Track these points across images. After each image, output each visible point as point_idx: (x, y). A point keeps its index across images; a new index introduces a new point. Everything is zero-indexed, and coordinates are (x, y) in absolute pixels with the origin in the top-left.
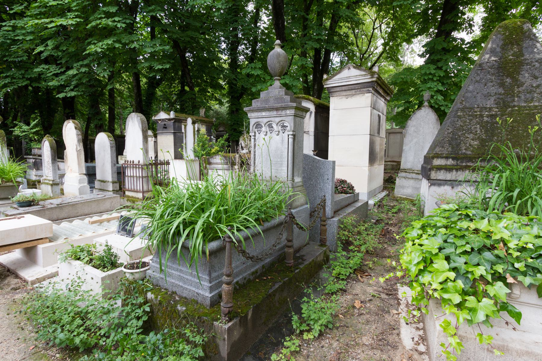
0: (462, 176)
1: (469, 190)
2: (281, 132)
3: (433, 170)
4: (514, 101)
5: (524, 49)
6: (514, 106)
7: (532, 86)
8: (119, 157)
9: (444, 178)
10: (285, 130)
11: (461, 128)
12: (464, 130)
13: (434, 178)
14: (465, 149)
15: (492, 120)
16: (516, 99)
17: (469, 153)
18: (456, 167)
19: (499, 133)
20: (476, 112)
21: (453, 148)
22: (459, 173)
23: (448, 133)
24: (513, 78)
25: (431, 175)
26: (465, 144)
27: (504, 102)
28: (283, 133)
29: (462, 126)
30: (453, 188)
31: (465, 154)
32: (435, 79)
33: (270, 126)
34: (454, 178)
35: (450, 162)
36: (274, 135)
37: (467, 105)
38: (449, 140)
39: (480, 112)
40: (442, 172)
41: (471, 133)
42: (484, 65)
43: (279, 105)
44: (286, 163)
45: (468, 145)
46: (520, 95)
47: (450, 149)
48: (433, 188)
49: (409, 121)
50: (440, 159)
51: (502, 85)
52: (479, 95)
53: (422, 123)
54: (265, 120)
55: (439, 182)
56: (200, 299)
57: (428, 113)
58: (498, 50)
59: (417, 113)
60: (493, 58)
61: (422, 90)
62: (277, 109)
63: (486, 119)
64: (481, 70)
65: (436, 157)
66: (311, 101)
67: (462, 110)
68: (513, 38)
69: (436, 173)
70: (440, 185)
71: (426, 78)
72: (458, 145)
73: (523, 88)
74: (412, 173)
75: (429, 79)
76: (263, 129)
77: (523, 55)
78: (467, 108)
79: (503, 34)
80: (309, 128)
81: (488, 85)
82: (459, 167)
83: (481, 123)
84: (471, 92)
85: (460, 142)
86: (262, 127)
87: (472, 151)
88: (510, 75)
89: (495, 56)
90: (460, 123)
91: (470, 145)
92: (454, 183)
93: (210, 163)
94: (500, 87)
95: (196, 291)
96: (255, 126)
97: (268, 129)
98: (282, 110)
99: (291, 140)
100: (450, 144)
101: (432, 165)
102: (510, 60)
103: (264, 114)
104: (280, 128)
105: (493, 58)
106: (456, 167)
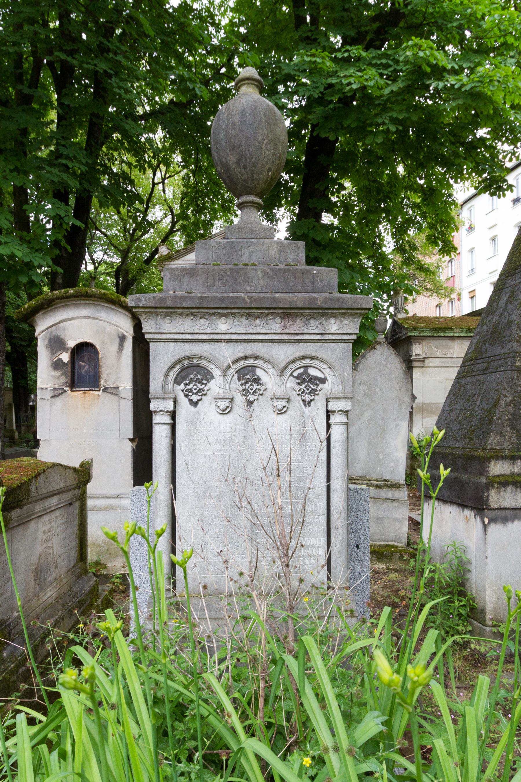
2: (297, 401)
3: (493, 487)
10: (313, 392)
13: (497, 506)
38: (509, 419)
40: (509, 489)
44: (323, 519)
47: (514, 439)
48: (495, 529)
50: (501, 462)
53: (379, 378)
55: (503, 513)
57: (387, 358)
69: (498, 493)
70: (505, 520)
80: (118, 378)
86: (208, 376)
96: (173, 374)
97: (236, 385)
100: (513, 428)
101: (488, 477)
104: (292, 383)
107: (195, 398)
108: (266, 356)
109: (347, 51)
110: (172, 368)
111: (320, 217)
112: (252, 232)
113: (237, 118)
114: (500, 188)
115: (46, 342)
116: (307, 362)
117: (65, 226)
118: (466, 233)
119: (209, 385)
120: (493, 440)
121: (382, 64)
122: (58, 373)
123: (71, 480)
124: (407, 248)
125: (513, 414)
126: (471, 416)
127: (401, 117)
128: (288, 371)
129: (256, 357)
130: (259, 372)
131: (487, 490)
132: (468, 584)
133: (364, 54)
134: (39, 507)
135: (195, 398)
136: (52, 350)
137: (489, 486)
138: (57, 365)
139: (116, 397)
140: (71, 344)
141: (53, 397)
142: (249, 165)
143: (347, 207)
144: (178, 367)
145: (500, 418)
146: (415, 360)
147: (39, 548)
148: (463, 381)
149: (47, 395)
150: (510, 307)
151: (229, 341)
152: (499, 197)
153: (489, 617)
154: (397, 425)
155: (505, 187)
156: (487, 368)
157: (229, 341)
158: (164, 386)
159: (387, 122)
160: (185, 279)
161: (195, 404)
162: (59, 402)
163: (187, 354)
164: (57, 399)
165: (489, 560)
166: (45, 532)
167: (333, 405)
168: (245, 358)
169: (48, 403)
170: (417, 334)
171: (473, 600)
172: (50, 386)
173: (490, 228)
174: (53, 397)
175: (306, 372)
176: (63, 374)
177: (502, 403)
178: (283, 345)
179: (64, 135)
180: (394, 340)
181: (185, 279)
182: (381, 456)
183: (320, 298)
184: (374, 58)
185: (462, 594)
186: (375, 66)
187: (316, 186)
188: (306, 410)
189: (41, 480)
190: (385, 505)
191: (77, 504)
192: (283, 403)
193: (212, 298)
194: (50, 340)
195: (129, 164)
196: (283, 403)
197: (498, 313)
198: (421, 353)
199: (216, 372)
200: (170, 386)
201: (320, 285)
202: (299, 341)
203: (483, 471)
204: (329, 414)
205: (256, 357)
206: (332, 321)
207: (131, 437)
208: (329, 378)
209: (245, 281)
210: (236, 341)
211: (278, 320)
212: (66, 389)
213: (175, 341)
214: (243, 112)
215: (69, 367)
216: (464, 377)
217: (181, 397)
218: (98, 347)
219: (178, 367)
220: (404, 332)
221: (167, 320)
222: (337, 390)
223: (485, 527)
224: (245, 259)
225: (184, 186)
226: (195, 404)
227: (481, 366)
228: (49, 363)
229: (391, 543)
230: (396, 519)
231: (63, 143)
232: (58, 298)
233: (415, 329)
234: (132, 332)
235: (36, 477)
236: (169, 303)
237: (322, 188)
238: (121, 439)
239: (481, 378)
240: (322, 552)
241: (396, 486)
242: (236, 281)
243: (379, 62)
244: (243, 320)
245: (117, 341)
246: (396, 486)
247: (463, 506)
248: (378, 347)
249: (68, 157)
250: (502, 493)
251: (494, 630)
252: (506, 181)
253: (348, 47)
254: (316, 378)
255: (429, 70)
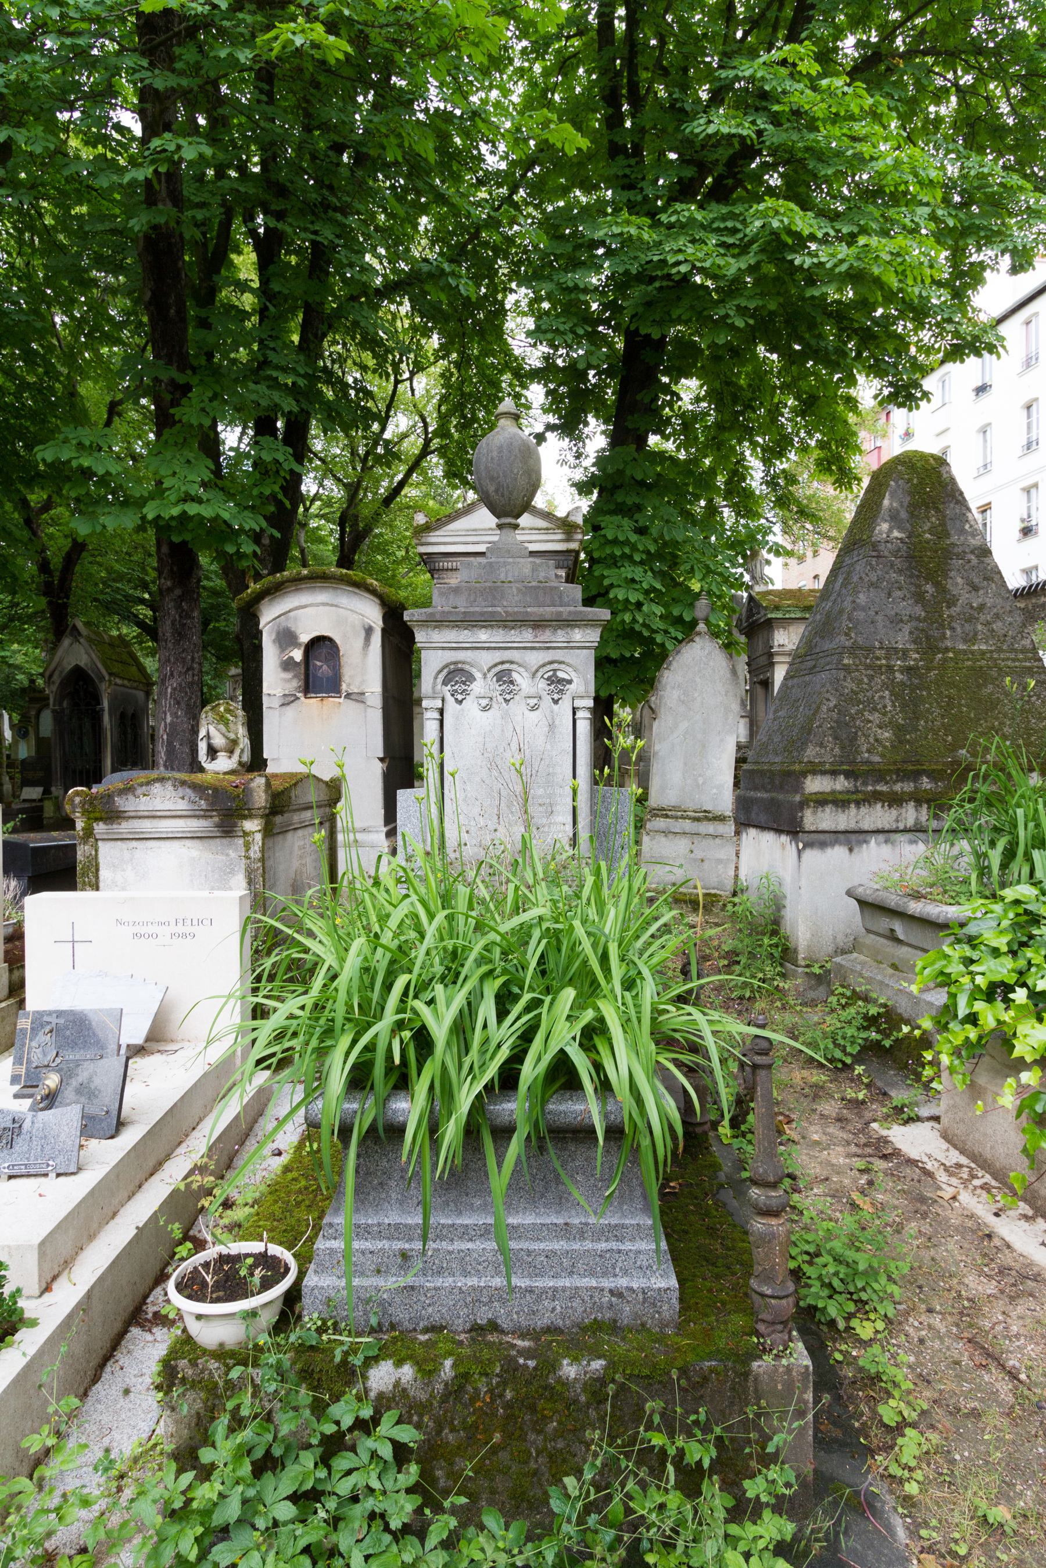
0: (878, 816)
1: (913, 851)
2: (547, 700)
4: (943, 637)
5: (949, 522)
6: (947, 650)
7: (972, 607)
8: (403, 796)
9: (833, 828)
10: (561, 691)
11: (852, 699)
12: (859, 702)
13: (813, 828)
14: (868, 751)
15: (910, 679)
16: (948, 632)
17: (877, 759)
18: (854, 797)
19: (928, 711)
20: (878, 659)
21: (842, 748)
22: (864, 810)
23: (829, 710)
24: (937, 584)
25: (805, 820)
26: (867, 736)
27: (928, 638)
28: (556, 702)
29: (856, 694)
30: (851, 850)
31: (868, 762)
32: (637, 558)
33: (504, 677)
34: (852, 826)
35: (841, 784)
36: (518, 707)
37: (860, 641)
38: (832, 728)
39: (887, 658)
40: (828, 809)
41: (875, 709)
42: (882, 547)
43: (548, 611)
45: (872, 740)
46: (954, 624)
47: (837, 751)
48: (810, 855)
49: (666, 673)
51: (919, 597)
52: (879, 618)
53: (698, 680)
54: (487, 659)
55: (822, 837)
56: (626, 1313)
57: (710, 653)
58: (904, 515)
59: (684, 650)
60: (896, 534)
61: (612, 586)
62: (538, 624)
63: (899, 676)
64: (878, 557)
65: (809, 772)
66: (373, 592)
67: (853, 650)
68: (926, 493)
69: (815, 813)
70: (823, 845)
71: (618, 553)
72: (853, 739)
73: (958, 609)
74: (683, 817)
75: (624, 556)
76: (478, 687)
77: (948, 535)
78: (861, 648)
79: (909, 481)
81: (894, 595)
82: (860, 796)
83: (890, 685)
84: (864, 609)
85: (856, 733)
86: (471, 678)
87: (882, 756)
88: (930, 577)
89: (901, 529)
90: (850, 685)
91: (877, 740)
92: (853, 837)
93: (113, 816)
94: (917, 602)
95: (607, 1283)
96: (441, 677)
98: (556, 629)
99: (584, 727)
100: (836, 738)
101: (803, 794)
102: (928, 542)
103: (483, 636)
104: (543, 684)
105: (896, 534)
106: (854, 797)
107: (460, 697)
108: (520, 661)
109: (675, 212)
110: (440, 671)
111: (645, 439)
112: (509, 551)
113: (495, 454)
114: (910, 397)
115: (274, 636)
116: (555, 666)
117: (282, 474)
118: (900, 441)
119: (472, 686)
120: (811, 752)
121: (726, 228)
122: (288, 675)
123: (324, 795)
124: (781, 482)
125: (836, 722)
126: (794, 725)
127: (752, 305)
128: (540, 674)
129: (512, 662)
130: (515, 675)
131: (802, 809)
132: (783, 922)
133: (699, 216)
134: (296, 818)
135: (460, 697)
136: (281, 646)
137: (803, 805)
138: (288, 665)
139: (362, 705)
140: (305, 638)
141: (283, 705)
142: (506, 493)
143: (688, 421)
144: (446, 671)
145: (820, 726)
146: (778, 654)
147: (296, 864)
148: (790, 683)
149: (276, 703)
150: (844, 591)
151: (488, 648)
152: (910, 410)
153: (801, 956)
154: (722, 740)
155: (919, 395)
156: (815, 666)
157: (488, 648)
158: (433, 688)
159: (732, 313)
160: (451, 597)
161: (460, 702)
162: (290, 711)
163: (453, 660)
164: (288, 708)
165: (802, 891)
166: (300, 848)
167: (578, 703)
168: (502, 663)
169: (277, 712)
170: (780, 616)
171: (787, 939)
172: (279, 692)
173: (938, 435)
174: (283, 705)
175: (555, 675)
176: (295, 676)
177: (824, 708)
178: (534, 652)
179: (274, 333)
180: (750, 625)
181: (451, 597)
182: (701, 781)
183: (565, 611)
184: (713, 221)
185: (774, 933)
186: (718, 230)
187: (639, 397)
188: (556, 707)
189: (298, 791)
190: (705, 842)
191: (327, 825)
192: (535, 701)
193: (474, 613)
194: (278, 633)
195: (364, 368)
196: (535, 701)
197: (832, 598)
198: (786, 642)
199: (478, 675)
200: (439, 687)
201: (566, 600)
202: (548, 648)
203: (798, 788)
204: (574, 711)
205: (512, 662)
206: (577, 630)
207: (381, 755)
208: (575, 680)
209: (502, 597)
210: (495, 648)
211: (530, 630)
212: (299, 695)
213: (443, 648)
214: (500, 449)
215: (303, 667)
216: (792, 677)
217: (448, 696)
218: (338, 641)
219: (446, 671)
220: (762, 613)
221: (436, 631)
222: (581, 690)
223: (799, 852)
224: (502, 577)
225: (443, 386)
226: (460, 702)
227: (810, 664)
228: (278, 662)
229: (713, 891)
230: (719, 861)
231: (272, 345)
232: (288, 581)
233: (777, 608)
234: (380, 623)
235: (295, 785)
236: (438, 618)
237: (647, 400)
238: (368, 758)
239: (807, 678)
240: (569, 829)
241: (720, 819)
242: (494, 598)
243: (722, 226)
244: (501, 631)
245: (363, 634)
246: (720, 819)
247: (779, 831)
248: (697, 639)
249: (277, 368)
250: (819, 814)
251: (807, 970)
252: (921, 386)
253: (678, 206)
254: (564, 680)
255: (790, 241)
